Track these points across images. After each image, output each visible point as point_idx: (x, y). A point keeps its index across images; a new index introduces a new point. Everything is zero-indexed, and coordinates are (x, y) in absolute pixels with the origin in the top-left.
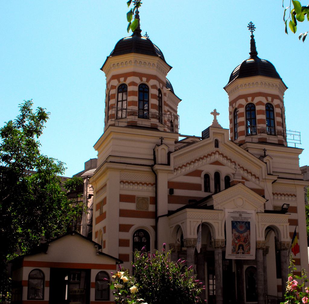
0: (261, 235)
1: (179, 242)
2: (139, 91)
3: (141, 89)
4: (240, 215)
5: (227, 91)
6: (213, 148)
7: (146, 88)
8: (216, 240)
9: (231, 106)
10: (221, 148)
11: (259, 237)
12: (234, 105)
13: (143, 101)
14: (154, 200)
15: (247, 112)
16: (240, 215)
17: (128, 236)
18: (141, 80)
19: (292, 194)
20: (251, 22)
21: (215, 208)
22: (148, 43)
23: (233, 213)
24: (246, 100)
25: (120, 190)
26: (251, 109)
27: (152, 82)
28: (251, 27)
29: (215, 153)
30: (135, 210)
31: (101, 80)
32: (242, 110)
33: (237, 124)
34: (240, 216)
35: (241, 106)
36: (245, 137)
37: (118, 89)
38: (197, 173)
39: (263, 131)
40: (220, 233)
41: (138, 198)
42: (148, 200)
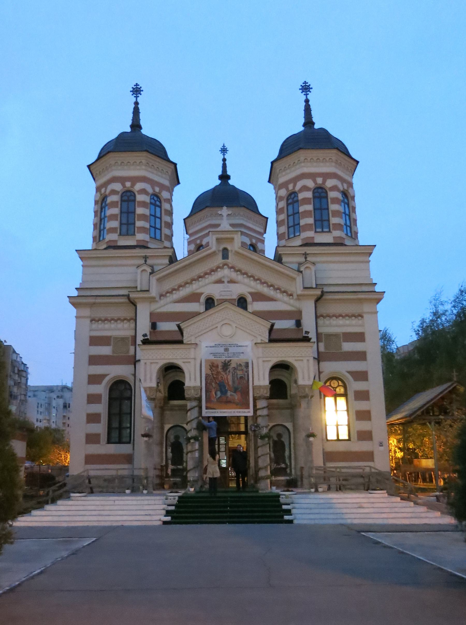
0: (193, 377)
1: (162, 393)
2: (314, 197)
3: (317, 194)
5: (93, 172)
6: (219, 260)
7: (324, 192)
8: (13, 394)
9: (98, 193)
10: (232, 260)
12: (103, 191)
13: (321, 209)
16: (226, 350)
17: (101, 389)
18: (314, 183)
19: (338, 315)
20: (305, 82)
21: (185, 342)
22: (324, 133)
23: (213, 347)
24: (307, 191)
25: (90, 330)
26: (128, 197)
27: (330, 183)
28: (306, 88)
29: (222, 268)
30: (111, 354)
32: (115, 198)
34: (225, 351)
35: (113, 192)
36: (117, 236)
37: (287, 200)
38: (193, 298)
41: (116, 338)
42: (129, 341)
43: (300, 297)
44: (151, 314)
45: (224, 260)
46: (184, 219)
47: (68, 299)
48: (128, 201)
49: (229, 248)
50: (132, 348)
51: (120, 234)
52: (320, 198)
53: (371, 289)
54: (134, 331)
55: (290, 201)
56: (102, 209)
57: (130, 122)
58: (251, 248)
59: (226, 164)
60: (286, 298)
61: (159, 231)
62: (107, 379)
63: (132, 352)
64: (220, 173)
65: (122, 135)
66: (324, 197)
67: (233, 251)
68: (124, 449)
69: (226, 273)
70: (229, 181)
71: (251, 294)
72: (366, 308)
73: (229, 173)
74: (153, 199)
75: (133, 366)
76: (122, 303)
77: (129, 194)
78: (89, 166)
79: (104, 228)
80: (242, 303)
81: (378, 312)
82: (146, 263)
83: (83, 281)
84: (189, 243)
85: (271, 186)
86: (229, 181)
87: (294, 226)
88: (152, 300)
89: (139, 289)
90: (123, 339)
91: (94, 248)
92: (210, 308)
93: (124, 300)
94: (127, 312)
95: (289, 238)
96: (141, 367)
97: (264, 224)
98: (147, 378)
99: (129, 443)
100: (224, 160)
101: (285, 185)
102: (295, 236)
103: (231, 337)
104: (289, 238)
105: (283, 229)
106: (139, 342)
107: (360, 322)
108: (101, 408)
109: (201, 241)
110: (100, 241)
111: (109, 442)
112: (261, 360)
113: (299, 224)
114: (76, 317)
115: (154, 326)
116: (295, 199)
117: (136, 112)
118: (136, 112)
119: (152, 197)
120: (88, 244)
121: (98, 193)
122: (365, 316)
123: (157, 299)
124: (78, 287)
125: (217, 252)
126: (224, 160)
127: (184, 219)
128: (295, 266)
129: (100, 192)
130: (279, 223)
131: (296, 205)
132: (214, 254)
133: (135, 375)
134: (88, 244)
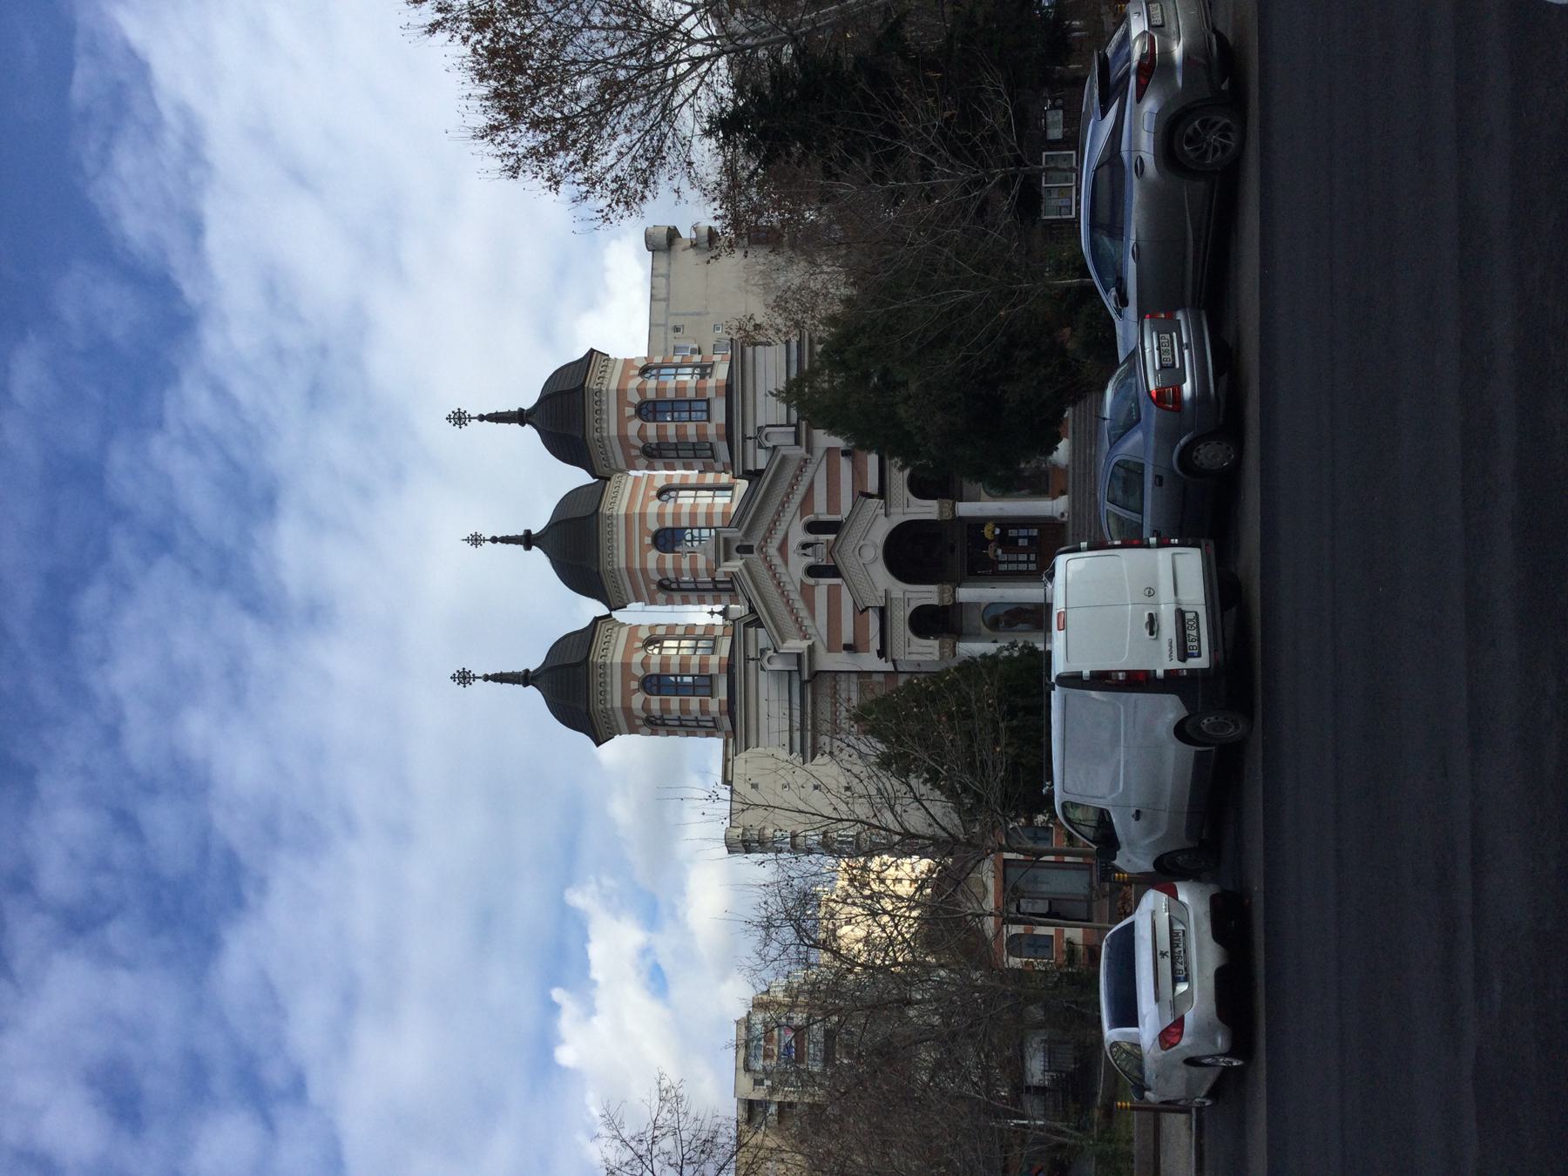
2: (655, 420)
14: (862, 674)
38: (807, 593)
43: (809, 450)
44: (829, 650)
48: (659, 686)
51: (712, 696)
52: (655, 412)
58: (665, 497)
60: (810, 469)
64: (520, 547)
69: (772, 550)
73: (521, 533)
76: (813, 694)
78: (598, 744)
84: (653, 602)
94: (825, 688)
95: (713, 457)
98: (925, 652)
100: (494, 540)
103: (876, 546)
104: (713, 457)
109: (653, 581)
117: (500, 678)
118: (500, 678)
126: (494, 540)
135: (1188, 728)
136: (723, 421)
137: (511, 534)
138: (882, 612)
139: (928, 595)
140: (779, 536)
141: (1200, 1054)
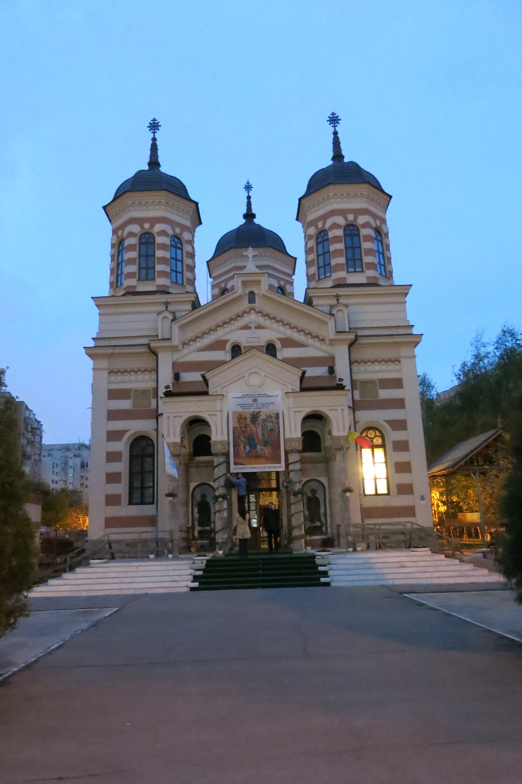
2: (345, 235)
3: (348, 232)
4: (255, 400)
5: (109, 213)
6: (245, 305)
9: (115, 236)
10: (259, 304)
11: (290, 431)
12: (120, 233)
15: (142, 246)
16: (255, 400)
17: (122, 446)
21: (210, 393)
23: (241, 398)
25: (109, 383)
26: (147, 240)
27: (362, 220)
28: (334, 120)
29: (248, 313)
30: (131, 408)
31: (104, 232)
33: (121, 263)
34: (253, 402)
37: (317, 239)
38: (219, 345)
39: (339, 267)
40: (219, 431)
41: (136, 391)
43: (332, 342)
44: (174, 364)
45: (250, 305)
46: (207, 262)
47: (84, 350)
48: (147, 243)
49: (256, 292)
50: (154, 401)
51: (139, 280)
53: (407, 331)
54: (156, 383)
55: (320, 240)
56: (119, 252)
57: (148, 160)
59: (250, 202)
60: (317, 344)
61: (180, 263)
62: (127, 435)
63: (153, 405)
64: (244, 211)
65: (140, 174)
66: (356, 235)
67: (261, 295)
68: (147, 510)
69: (253, 317)
70: (255, 220)
71: (280, 340)
72: (403, 352)
73: (254, 211)
74: (174, 241)
75: (155, 420)
77: (351, 228)
78: (104, 208)
79: (122, 273)
80: (271, 349)
81: (416, 356)
82: (167, 310)
83: (101, 331)
84: (213, 287)
85: (299, 225)
86: (255, 220)
87: (324, 266)
88: (175, 349)
89: (160, 338)
90: (144, 392)
91: (111, 295)
92: (237, 356)
93: (145, 349)
94: (147, 362)
95: (319, 279)
96: (163, 421)
97: (293, 265)
98: (170, 432)
99: (152, 503)
100: (249, 198)
101: (314, 223)
102: (325, 277)
103: (260, 386)
104: (319, 279)
105: (313, 270)
106: (161, 394)
107: (397, 367)
108: (122, 467)
109: (226, 284)
110: (117, 287)
111: (131, 502)
112: (292, 411)
113: (330, 264)
114: (93, 369)
115: (177, 377)
116: (325, 237)
117: (154, 148)
119: (173, 239)
120: (105, 291)
121: (115, 236)
122: (402, 360)
123: (180, 347)
124: (95, 337)
125: (243, 296)
126: (249, 198)
127: (207, 262)
128: (327, 309)
129: (117, 234)
130: (308, 264)
131: (326, 244)
132: (239, 298)
133: (157, 430)
134: (105, 291)
135: (388, 199)
136: (348, 282)
137: (253, 207)
138: (206, 393)
139: (169, 390)
140: (268, 323)
141: (99, 537)
